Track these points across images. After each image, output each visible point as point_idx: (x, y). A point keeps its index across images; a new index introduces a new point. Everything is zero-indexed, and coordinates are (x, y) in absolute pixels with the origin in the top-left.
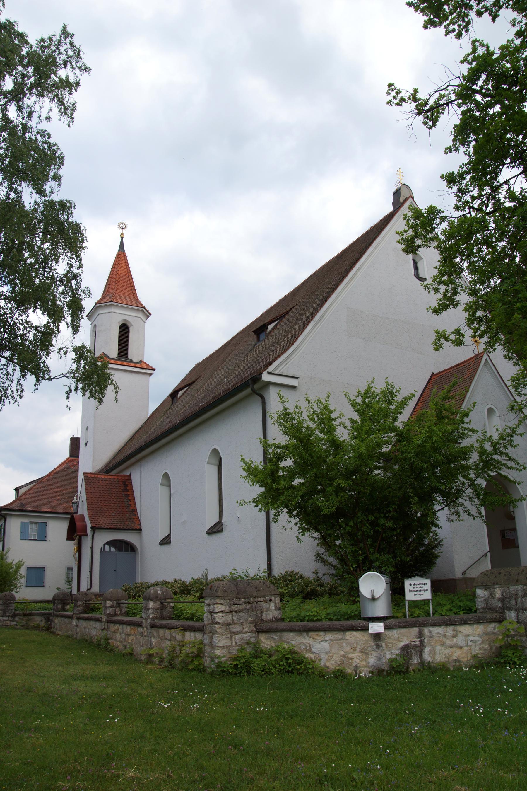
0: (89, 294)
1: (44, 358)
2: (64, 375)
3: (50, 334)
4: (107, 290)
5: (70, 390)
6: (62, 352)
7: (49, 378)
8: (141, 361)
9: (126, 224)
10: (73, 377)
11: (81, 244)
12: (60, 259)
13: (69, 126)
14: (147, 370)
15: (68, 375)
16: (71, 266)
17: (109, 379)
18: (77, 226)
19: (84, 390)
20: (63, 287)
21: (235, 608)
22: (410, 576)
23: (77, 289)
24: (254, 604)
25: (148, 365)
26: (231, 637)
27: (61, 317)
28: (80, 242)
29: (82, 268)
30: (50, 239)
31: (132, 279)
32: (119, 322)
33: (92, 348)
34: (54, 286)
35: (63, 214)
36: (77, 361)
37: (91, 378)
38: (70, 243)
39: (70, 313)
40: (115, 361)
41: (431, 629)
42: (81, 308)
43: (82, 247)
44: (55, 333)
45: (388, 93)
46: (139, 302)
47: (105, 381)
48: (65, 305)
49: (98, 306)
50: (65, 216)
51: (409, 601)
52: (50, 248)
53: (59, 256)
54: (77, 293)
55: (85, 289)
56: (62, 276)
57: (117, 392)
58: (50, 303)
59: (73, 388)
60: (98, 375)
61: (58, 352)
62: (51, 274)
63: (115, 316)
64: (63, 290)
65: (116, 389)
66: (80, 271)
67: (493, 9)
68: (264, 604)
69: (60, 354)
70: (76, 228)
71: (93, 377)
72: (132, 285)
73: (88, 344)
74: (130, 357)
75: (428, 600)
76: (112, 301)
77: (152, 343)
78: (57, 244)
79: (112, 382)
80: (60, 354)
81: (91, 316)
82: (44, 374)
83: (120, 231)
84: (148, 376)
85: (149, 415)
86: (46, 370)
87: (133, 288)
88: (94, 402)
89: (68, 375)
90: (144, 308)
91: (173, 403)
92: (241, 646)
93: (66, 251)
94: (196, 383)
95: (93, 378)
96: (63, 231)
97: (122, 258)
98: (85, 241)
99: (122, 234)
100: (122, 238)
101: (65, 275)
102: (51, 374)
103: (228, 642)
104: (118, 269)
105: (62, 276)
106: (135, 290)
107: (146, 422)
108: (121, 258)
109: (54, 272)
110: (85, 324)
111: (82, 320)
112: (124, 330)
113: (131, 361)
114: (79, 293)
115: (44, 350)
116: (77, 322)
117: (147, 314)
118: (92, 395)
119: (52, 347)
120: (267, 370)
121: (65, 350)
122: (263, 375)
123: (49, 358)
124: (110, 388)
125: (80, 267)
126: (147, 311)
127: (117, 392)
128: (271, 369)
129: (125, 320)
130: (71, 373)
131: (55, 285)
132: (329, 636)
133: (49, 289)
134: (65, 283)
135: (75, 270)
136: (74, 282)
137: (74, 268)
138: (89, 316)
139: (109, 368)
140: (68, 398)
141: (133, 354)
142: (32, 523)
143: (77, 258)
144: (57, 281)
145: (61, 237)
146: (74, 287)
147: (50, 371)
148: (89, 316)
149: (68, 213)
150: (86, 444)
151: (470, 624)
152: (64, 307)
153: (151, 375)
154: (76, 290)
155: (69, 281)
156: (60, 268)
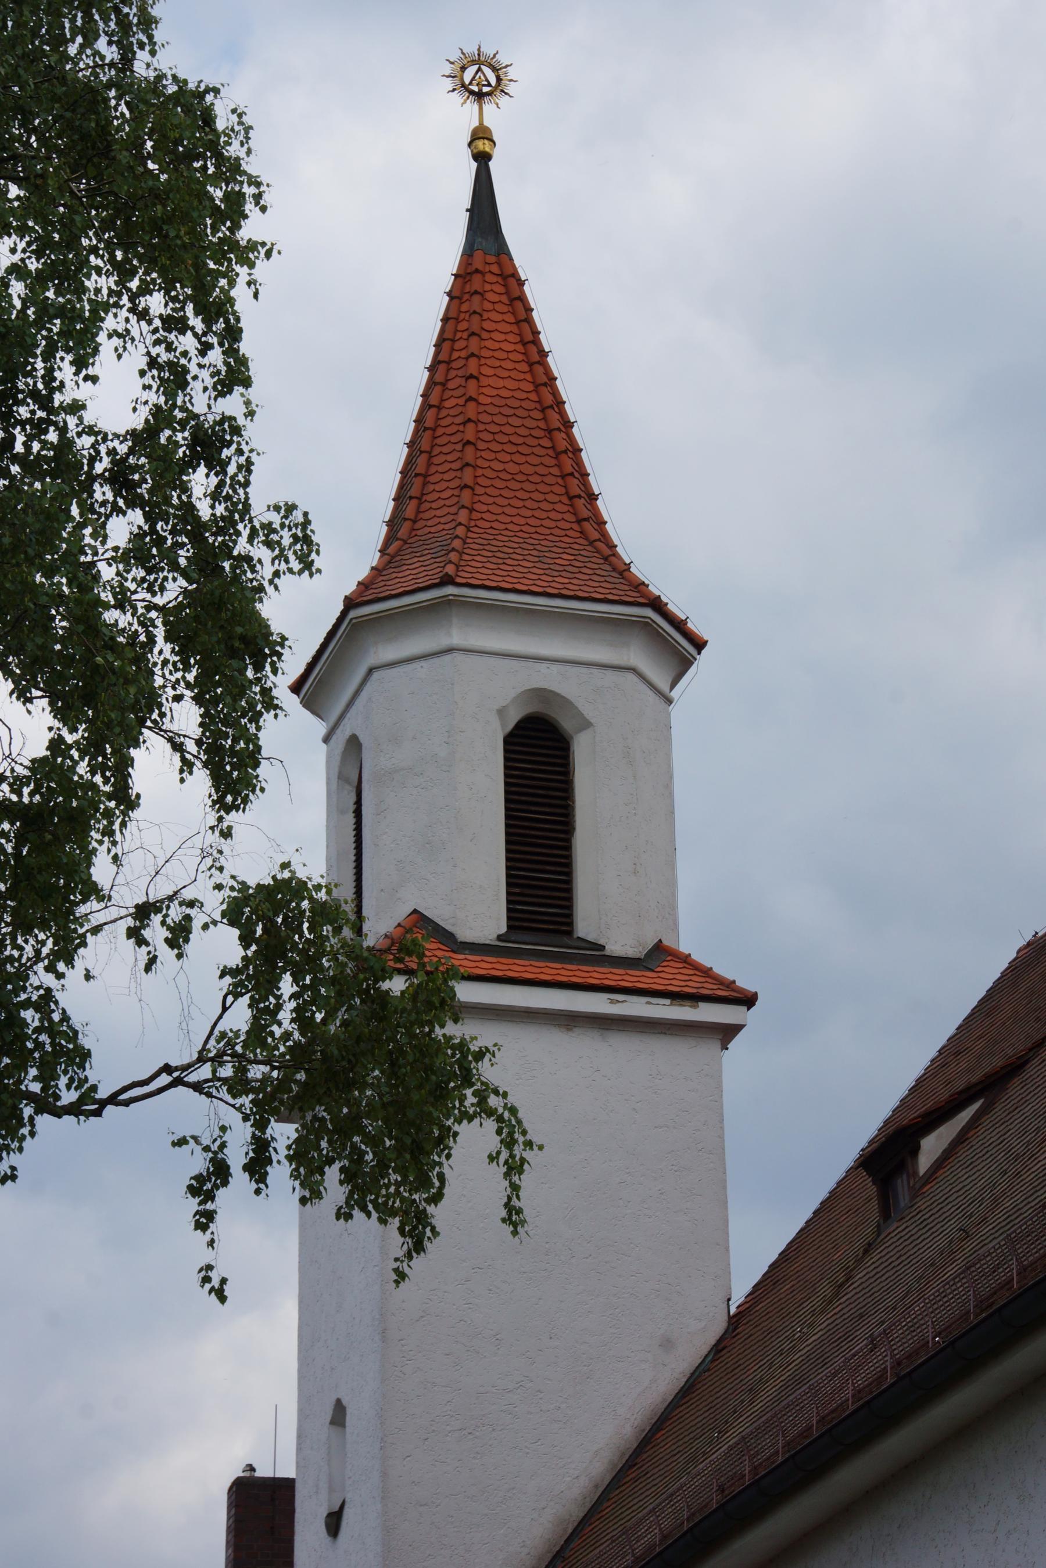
0: (305, 551)
1: (41, 977)
2: (176, 1076)
3: (77, 824)
4: (410, 511)
5: (220, 1171)
6: (156, 932)
7: (82, 1100)
8: (660, 952)
9: (503, 59)
10: (238, 1085)
11: (224, 231)
12: (102, 338)
14: (691, 999)
15: (205, 1072)
16: (174, 378)
17: (467, 1079)
18: (188, 110)
19: (307, 1164)
20: (137, 517)
23: (226, 526)
25: (707, 973)
27: (135, 708)
28: (219, 217)
29: (247, 383)
30: (27, 208)
31: (568, 425)
32: (501, 712)
33: (345, 892)
34: (75, 511)
35: (90, 36)
36: (253, 979)
37: (351, 1085)
38: (156, 226)
39: (191, 677)
40: (496, 960)
42: (260, 645)
43: (233, 245)
44: (108, 814)
46: (623, 570)
47: (441, 1095)
48: (160, 633)
49: (362, 616)
50: (102, 44)
52: (33, 265)
53: (96, 318)
54: (226, 551)
55: (275, 519)
56: (123, 449)
57: (514, 1168)
58: (61, 624)
59: (237, 1156)
60: (393, 1062)
61: (135, 934)
62: (52, 436)
63: (471, 677)
64: (137, 537)
65: (509, 1143)
66: (232, 405)
69: (141, 942)
70: (187, 120)
71: (356, 1073)
72: (568, 465)
73: (314, 866)
74: (585, 927)
76: (447, 581)
77: (723, 821)
78: (71, 242)
79: (482, 1097)
80: (141, 942)
81: (321, 683)
82: (47, 1077)
83: (465, 115)
84: (709, 1048)
85: (740, 1292)
86: (58, 1052)
87: (574, 483)
88: (374, 1237)
89: (205, 1072)
90: (657, 605)
91: (886, 1212)
93: (134, 284)
94: (1032, 1069)
95: (363, 1086)
96: (106, 153)
97: (495, 293)
98: (249, 207)
99: (481, 133)
100: (482, 159)
101: (142, 439)
102: (93, 1073)
104: (473, 367)
105: (123, 449)
106: (593, 497)
107: (719, 1348)
108: (487, 290)
109: (72, 421)
110: (292, 741)
111: (268, 717)
112: (539, 757)
113: (594, 953)
114: (242, 546)
115: (44, 927)
116: (243, 734)
117: (678, 644)
118: (363, 1192)
119: (93, 905)
121: (175, 913)
123: (74, 976)
124: (473, 1142)
125: (235, 376)
126: (680, 625)
127: (514, 1168)
129: (541, 694)
130: (218, 1060)
131: (87, 509)
133: (48, 538)
134: (143, 490)
135: (199, 399)
136: (200, 481)
137: (195, 388)
138: (311, 688)
139: (460, 1012)
140: (204, 1220)
141: (605, 908)
143: (208, 322)
144: (92, 478)
145: (91, 193)
146: (204, 510)
147: (86, 1055)
148: (311, 688)
149: (124, 24)
150: (334, 1522)
152: (151, 640)
153: (727, 1033)
154: (221, 531)
155: (171, 473)
156: (111, 395)
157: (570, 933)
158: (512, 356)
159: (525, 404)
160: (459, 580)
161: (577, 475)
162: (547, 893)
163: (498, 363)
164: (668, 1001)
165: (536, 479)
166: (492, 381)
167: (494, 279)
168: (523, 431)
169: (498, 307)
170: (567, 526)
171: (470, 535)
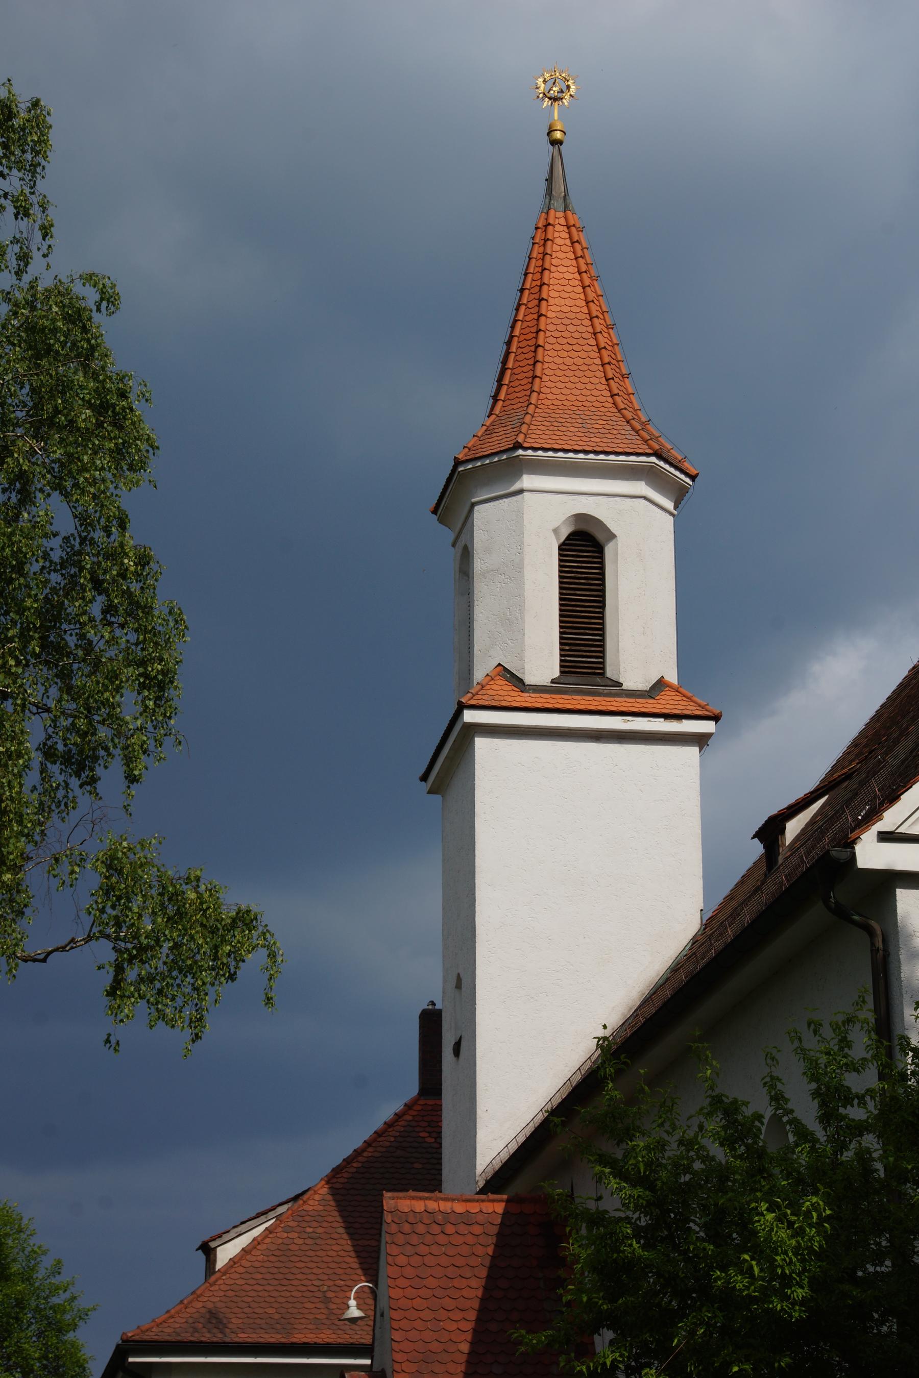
32: (556, 531)
67: (92, 490)
120: (880, 826)
122: (858, 848)
128: (890, 819)
129: (580, 518)
157: (603, 674)
158: (571, 282)
159: (578, 316)
160: (526, 445)
161: (614, 362)
162: (587, 648)
163: (561, 288)
164: (662, 720)
165: (584, 368)
166: (557, 301)
167: (562, 228)
168: (577, 335)
169: (563, 248)
170: (604, 399)
171: (537, 410)
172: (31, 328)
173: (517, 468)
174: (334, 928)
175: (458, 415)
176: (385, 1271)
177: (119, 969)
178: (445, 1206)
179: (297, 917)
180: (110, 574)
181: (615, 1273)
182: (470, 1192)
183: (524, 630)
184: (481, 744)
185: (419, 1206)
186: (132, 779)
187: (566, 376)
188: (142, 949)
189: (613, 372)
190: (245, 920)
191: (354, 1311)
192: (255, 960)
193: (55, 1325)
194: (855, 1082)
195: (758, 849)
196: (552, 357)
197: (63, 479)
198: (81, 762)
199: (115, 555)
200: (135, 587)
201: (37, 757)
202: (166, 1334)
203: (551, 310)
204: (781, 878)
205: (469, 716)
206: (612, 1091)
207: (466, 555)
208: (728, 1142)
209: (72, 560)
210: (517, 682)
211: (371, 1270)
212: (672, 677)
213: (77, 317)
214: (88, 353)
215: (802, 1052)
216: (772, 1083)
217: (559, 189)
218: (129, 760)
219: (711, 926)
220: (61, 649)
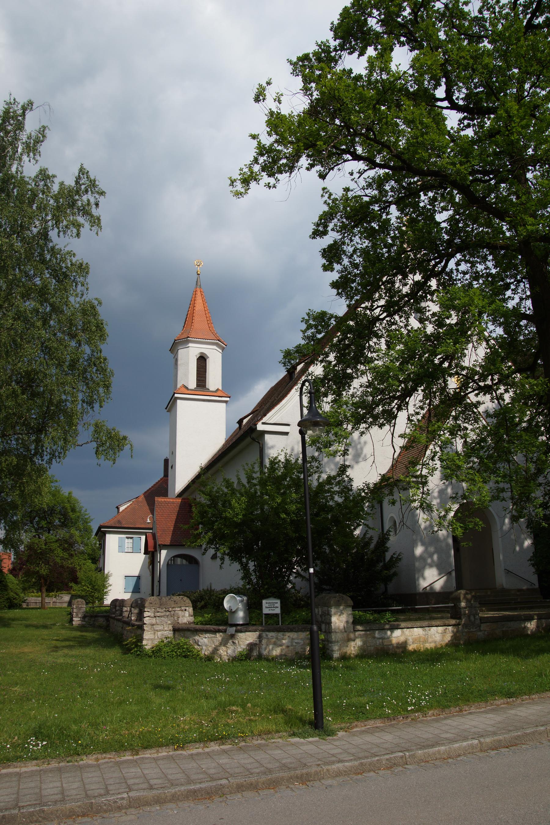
13: (97, 233)
21: (158, 614)
22: (267, 597)
24: (172, 613)
26: (155, 633)
41: (267, 633)
45: (322, 196)
51: (265, 614)
68: (180, 612)
75: (277, 615)
92: (161, 639)
103: (152, 636)
128: (265, 419)
129: (201, 353)
132: (208, 635)
142: (128, 538)
151: (295, 631)
172: (83, 309)
173: (188, 342)
174: (142, 440)
175: (177, 331)
176: (155, 513)
177: (97, 448)
178: (168, 500)
179: (135, 437)
180: (98, 363)
181: (203, 514)
182: (174, 497)
183: (188, 376)
184: (178, 401)
185: (163, 500)
186: (101, 407)
187: (199, 322)
188: (103, 444)
189: (209, 323)
190: (125, 438)
191: (149, 521)
192: (127, 447)
193: (86, 522)
194: (255, 475)
195: (237, 425)
196: (196, 319)
197: (89, 342)
198: (90, 403)
199: (99, 358)
200: (103, 365)
201: (81, 402)
202: (109, 525)
203: (196, 309)
204: (242, 432)
205: (176, 395)
206: (203, 478)
207: (177, 360)
208: (227, 487)
209: (90, 359)
210: (187, 388)
211: (152, 512)
212: (220, 388)
213: (93, 307)
214: (95, 314)
215: (244, 469)
216: (237, 476)
217: (199, 284)
218: (101, 402)
219: (227, 442)
220: (86, 378)
